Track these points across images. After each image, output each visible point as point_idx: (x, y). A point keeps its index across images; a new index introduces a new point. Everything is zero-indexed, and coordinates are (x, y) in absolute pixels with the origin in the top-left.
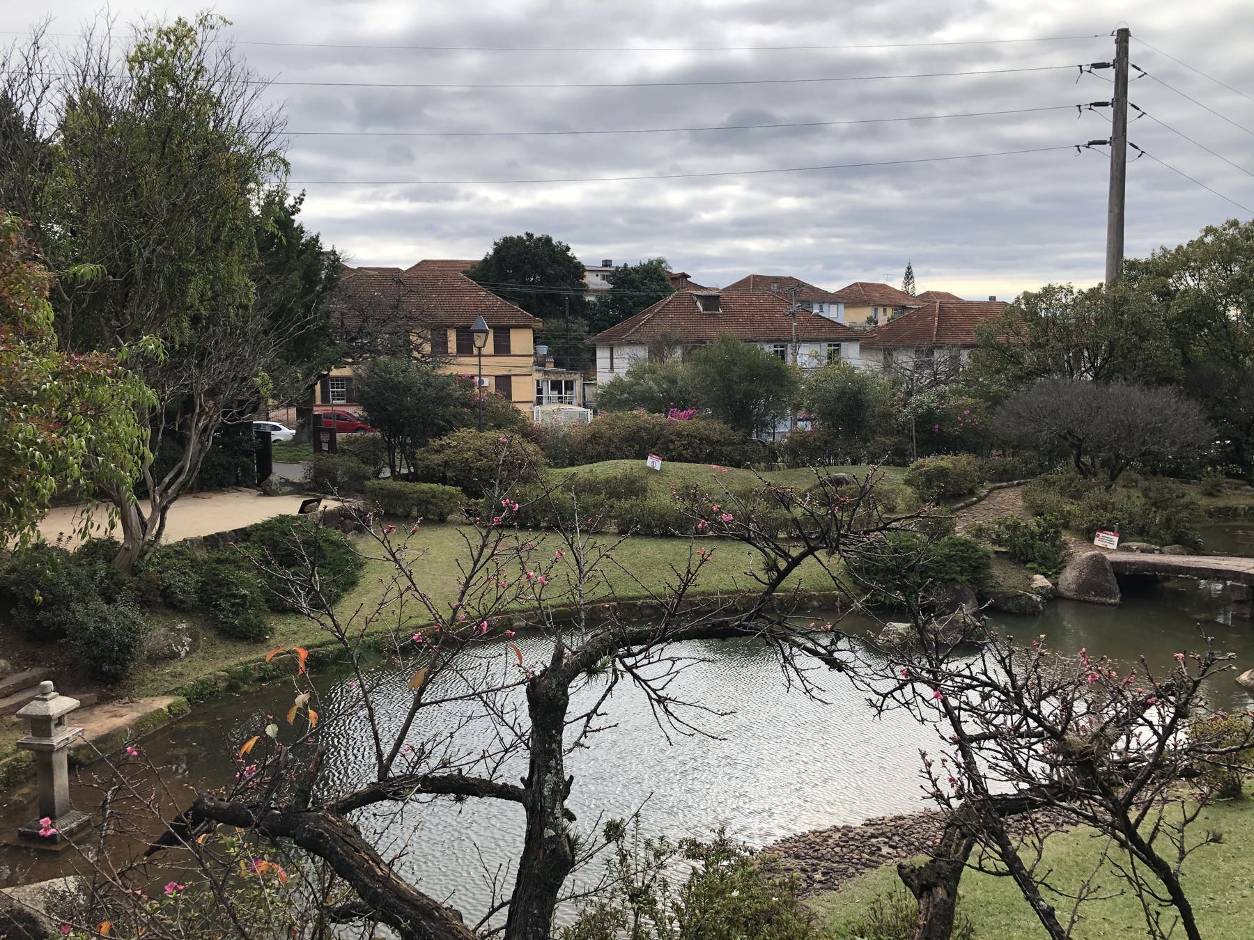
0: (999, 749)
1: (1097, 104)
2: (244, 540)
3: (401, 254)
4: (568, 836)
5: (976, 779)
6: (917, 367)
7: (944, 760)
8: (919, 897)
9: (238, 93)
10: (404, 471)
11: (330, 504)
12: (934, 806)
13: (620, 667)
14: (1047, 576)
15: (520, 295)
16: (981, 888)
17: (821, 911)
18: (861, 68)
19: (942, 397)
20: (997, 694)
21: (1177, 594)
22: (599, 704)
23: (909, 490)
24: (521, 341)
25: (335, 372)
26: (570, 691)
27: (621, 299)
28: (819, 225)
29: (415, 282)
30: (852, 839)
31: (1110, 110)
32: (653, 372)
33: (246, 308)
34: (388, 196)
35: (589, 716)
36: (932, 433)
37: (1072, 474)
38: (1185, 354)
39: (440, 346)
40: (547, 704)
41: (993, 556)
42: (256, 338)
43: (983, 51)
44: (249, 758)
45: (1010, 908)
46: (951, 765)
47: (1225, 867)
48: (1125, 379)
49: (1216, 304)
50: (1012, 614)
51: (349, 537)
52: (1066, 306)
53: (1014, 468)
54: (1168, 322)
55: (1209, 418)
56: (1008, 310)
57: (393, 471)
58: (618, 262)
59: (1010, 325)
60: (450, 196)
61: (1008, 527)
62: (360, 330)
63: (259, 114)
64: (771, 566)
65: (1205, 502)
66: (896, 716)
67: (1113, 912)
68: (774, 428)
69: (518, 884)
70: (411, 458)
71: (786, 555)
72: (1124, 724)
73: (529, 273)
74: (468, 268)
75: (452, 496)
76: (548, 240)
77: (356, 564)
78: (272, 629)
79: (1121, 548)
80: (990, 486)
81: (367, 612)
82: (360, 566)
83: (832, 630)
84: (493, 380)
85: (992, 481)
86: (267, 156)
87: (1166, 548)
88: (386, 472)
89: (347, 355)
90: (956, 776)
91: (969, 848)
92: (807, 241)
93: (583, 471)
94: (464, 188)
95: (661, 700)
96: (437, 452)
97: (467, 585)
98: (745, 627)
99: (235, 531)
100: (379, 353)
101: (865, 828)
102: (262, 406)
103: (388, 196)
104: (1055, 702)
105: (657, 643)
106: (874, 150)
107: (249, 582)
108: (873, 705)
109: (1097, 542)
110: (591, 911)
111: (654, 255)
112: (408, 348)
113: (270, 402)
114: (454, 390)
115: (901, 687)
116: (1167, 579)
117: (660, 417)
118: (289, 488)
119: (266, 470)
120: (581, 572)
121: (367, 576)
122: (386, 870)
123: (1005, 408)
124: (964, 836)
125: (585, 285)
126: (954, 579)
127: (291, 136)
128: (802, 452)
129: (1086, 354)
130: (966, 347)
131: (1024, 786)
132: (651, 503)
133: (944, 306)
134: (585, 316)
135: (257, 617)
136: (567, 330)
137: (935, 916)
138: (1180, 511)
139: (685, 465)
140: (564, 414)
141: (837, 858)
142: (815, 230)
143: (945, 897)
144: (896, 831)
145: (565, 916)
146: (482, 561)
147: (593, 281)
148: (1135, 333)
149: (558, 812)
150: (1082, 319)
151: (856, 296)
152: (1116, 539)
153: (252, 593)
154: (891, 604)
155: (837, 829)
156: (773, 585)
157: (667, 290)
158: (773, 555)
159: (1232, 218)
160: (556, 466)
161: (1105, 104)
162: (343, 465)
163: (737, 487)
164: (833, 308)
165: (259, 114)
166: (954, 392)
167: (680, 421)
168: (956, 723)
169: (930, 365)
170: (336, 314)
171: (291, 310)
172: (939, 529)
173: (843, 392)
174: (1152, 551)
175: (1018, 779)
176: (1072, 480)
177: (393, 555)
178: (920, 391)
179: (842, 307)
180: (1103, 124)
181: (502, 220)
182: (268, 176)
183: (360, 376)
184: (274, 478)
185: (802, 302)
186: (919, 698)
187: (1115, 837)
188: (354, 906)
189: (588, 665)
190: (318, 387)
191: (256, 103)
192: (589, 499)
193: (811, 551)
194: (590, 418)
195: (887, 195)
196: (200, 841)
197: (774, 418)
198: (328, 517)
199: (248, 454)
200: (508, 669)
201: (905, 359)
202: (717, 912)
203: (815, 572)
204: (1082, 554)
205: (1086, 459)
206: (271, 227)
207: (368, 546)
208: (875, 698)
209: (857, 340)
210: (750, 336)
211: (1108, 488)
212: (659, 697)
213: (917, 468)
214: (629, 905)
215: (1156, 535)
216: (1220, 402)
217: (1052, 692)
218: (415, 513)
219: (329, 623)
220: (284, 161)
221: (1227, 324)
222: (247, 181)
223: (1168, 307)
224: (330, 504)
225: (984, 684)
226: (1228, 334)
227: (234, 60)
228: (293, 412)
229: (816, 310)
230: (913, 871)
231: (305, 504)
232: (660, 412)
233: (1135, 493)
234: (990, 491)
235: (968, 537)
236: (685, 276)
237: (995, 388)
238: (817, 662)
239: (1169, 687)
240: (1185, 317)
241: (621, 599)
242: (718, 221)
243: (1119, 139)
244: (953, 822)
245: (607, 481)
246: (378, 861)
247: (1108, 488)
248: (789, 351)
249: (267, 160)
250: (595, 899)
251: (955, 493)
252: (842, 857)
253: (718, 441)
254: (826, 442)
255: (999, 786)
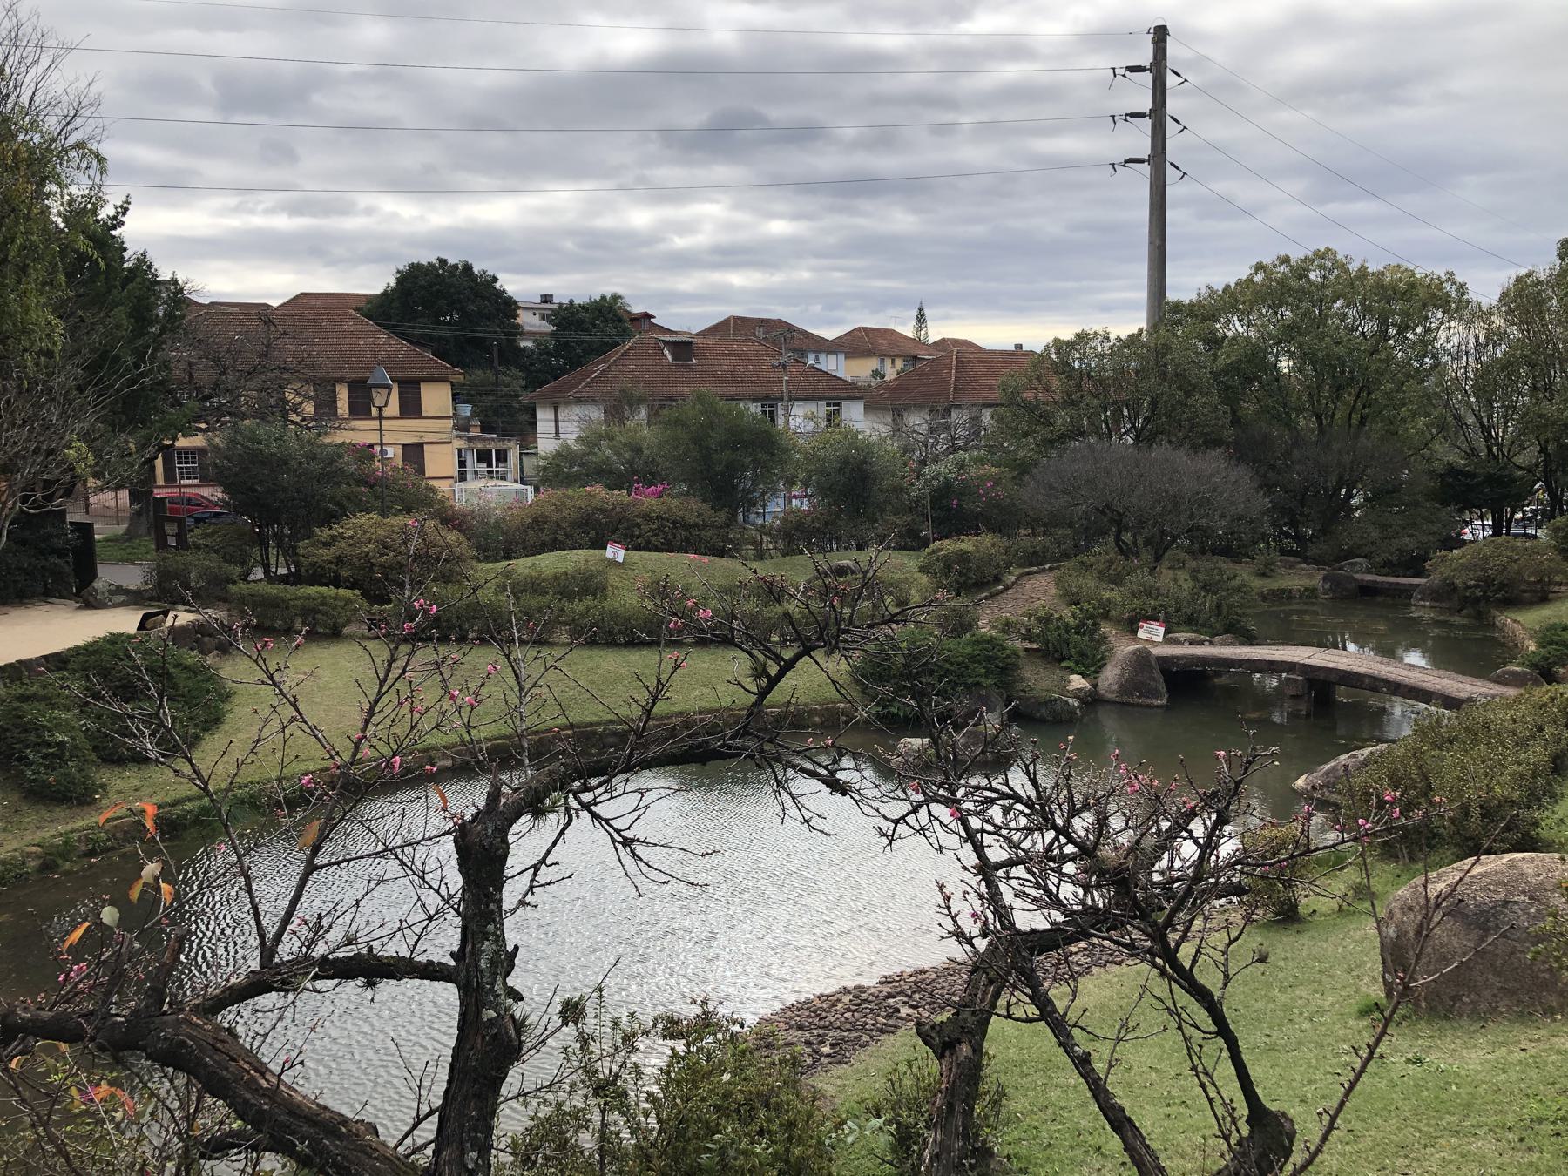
0: (1029, 877)
1: (1133, 115)
2: (59, 669)
3: (272, 285)
4: (512, 1016)
5: (1003, 912)
6: (932, 430)
7: (965, 893)
8: (940, 1057)
9: (29, 61)
10: (282, 571)
11: (183, 617)
12: (958, 951)
13: (574, 804)
14: (1084, 676)
15: (431, 338)
16: (1012, 1040)
17: (830, 1090)
18: (871, 62)
19: (961, 466)
20: (1019, 806)
21: (1230, 693)
22: (549, 852)
23: (925, 579)
24: (436, 398)
25: (182, 442)
26: (511, 839)
27: (567, 344)
28: (818, 254)
29: (289, 322)
30: (865, 1001)
31: (1147, 122)
32: (612, 438)
33: (49, 354)
34: (261, 207)
35: (536, 868)
36: (950, 511)
37: (1112, 555)
38: (1234, 412)
39: (326, 406)
40: (482, 857)
41: (1022, 654)
42: (66, 395)
43: (1016, 49)
44: (77, 952)
45: (1047, 1067)
46: (972, 896)
47: (1282, 998)
48: (1170, 442)
49: (1266, 353)
50: (1041, 720)
51: (210, 660)
52: (1103, 355)
53: (1046, 550)
54: (1216, 375)
55: (1261, 487)
56: (1037, 359)
57: (267, 571)
58: (562, 296)
59: (1039, 379)
60: (346, 210)
61: (1039, 620)
62: (217, 385)
63: (60, 89)
64: (759, 672)
65: (1258, 583)
66: (911, 845)
67: (1160, 1060)
68: (764, 506)
69: (449, 1082)
70: (290, 553)
71: (777, 658)
72: (1166, 843)
73: (444, 312)
74: (362, 304)
75: (348, 602)
76: (468, 268)
77: (220, 695)
78: (103, 786)
79: (1168, 640)
80: (1018, 572)
81: (237, 753)
82: (227, 697)
83: (833, 746)
84: (399, 450)
85: (1020, 566)
86: (73, 147)
87: (1217, 639)
88: (258, 573)
89: (198, 419)
90: (978, 909)
91: (997, 995)
92: (804, 275)
93: (523, 566)
94: (364, 200)
95: (627, 843)
96: (326, 545)
97: (371, 713)
98: (729, 747)
99: (45, 657)
100: (243, 417)
101: (880, 987)
102: (79, 487)
103: (261, 207)
104: (1089, 818)
105: (621, 772)
106: (885, 163)
107: (67, 725)
108: (882, 833)
109: (1141, 634)
110: (545, 1111)
111: (608, 291)
112: (283, 409)
113: (91, 482)
114: (347, 463)
115: (915, 811)
116: (1218, 674)
117: (620, 495)
118: (122, 598)
119: (86, 574)
120: (521, 689)
121: (236, 709)
122: (274, 1081)
123: (1033, 477)
124: (991, 982)
125: (519, 326)
126: (978, 684)
127: (107, 122)
128: (795, 536)
129: (1126, 412)
130: (988, 405)
131: (1058, 917)
132: (612, 603)
133: (961, 355)
134: (519, 367)
135: (81, 770)
136: (497, 384)
137: (958, 1077)
138: (1231, 595)
139: (654, 555)
140: (495, 493)
141: (848, 1026)
142: (813, 262)
143: (970, 1053)
144: (917, 986)
145: (512, 1121)
146: (389, 682)
147: (529, 321)
148: (1180, 388)
149: (498, 988)
150: (1121, 372)
151: (859, 343)
152: (1162, 630)
153: (73, 739)
154: (905, 716)
155: (847, 991)
156: (763, 694)
157: (625, 334)
158: (761, 658)
159: (1282, 254)
160: (487, 560)
161: (1142, 115)
162: (198, 564)
163: (721, 581)
164: (832, 358)
165: (60, 89)
166: (975, 461)
167: (646, 500)
168: (979, 849)
169: (947, 427)
170: (182, 365)
171: (116, 359)
172: (960, 625)
173: (846, 462)
174: (1201, 643)
175: (1048, 906)
176: (1111, 562)
177: (271, 678)
178: (936, 459)
179: (841, 357)
180: (1139, 140)
181: (412, 241)
182: (74, 174)
183: (217, 448)
184: (99, 584)
185: (794, 351)
186: (936, 823)
187: (1154, 965)
188: (232, 1134)
189: (535, 805)
190: (159, 463)
191: (55, 75)
192: (533, 601)
193: (807, 651)
194: (530, 496)
195: (900, 220)
196: (13, 1065)
197: (763, 494)
198: (178, 634)
199: (61, 554)
200: (427, 822)
201: (918, 421)
202: (703, 1099)
203: (813, 680)
204: (1124, 649)
205: (1127, 537)
206: (82, 243)
207: (236, 671)
208: (884, 825)
209: (860, 398)
210: (732, 393)
211: (1152, 570)
212: (625, 838)
213: (933, 552)
214: (593, 1101)
215: (1204, 625)
216: (1273, 467)
217: (1086, 807)
218: (298, 625)
219: (187, 770)
220: (97, 155)
221: (1279, 377)
222: (42, 182)
223: (1216, 356)
224: (183, 617)
225: (1004, 796)
226: (1280, 388)
227: (23, 16)
228: (124, 496)
229: (811, 361)
230: (933, 1027)
231: (145, 618)
232: (621, 488)
233: (1183, 576)
234: (1018, 578)
235: (994, 633)
236: (648, 316)
237: (1022, 454)
238: (815, 785)
239: (1214, 794)
240: (1234, 369)
241: (578, 726)
242: (694, 248)
243: (1158, 157)
244: (979, 966)
245: (555, 578)
246: (262, 1070)
247: (1152, 570)
248: (780, 412)
249: (73, 154)
250: (550, 1096)
251: (975, 580)
252: (854, 1024)
253: (695, 525)
254: (826, 524)
255: (1029, 919)
